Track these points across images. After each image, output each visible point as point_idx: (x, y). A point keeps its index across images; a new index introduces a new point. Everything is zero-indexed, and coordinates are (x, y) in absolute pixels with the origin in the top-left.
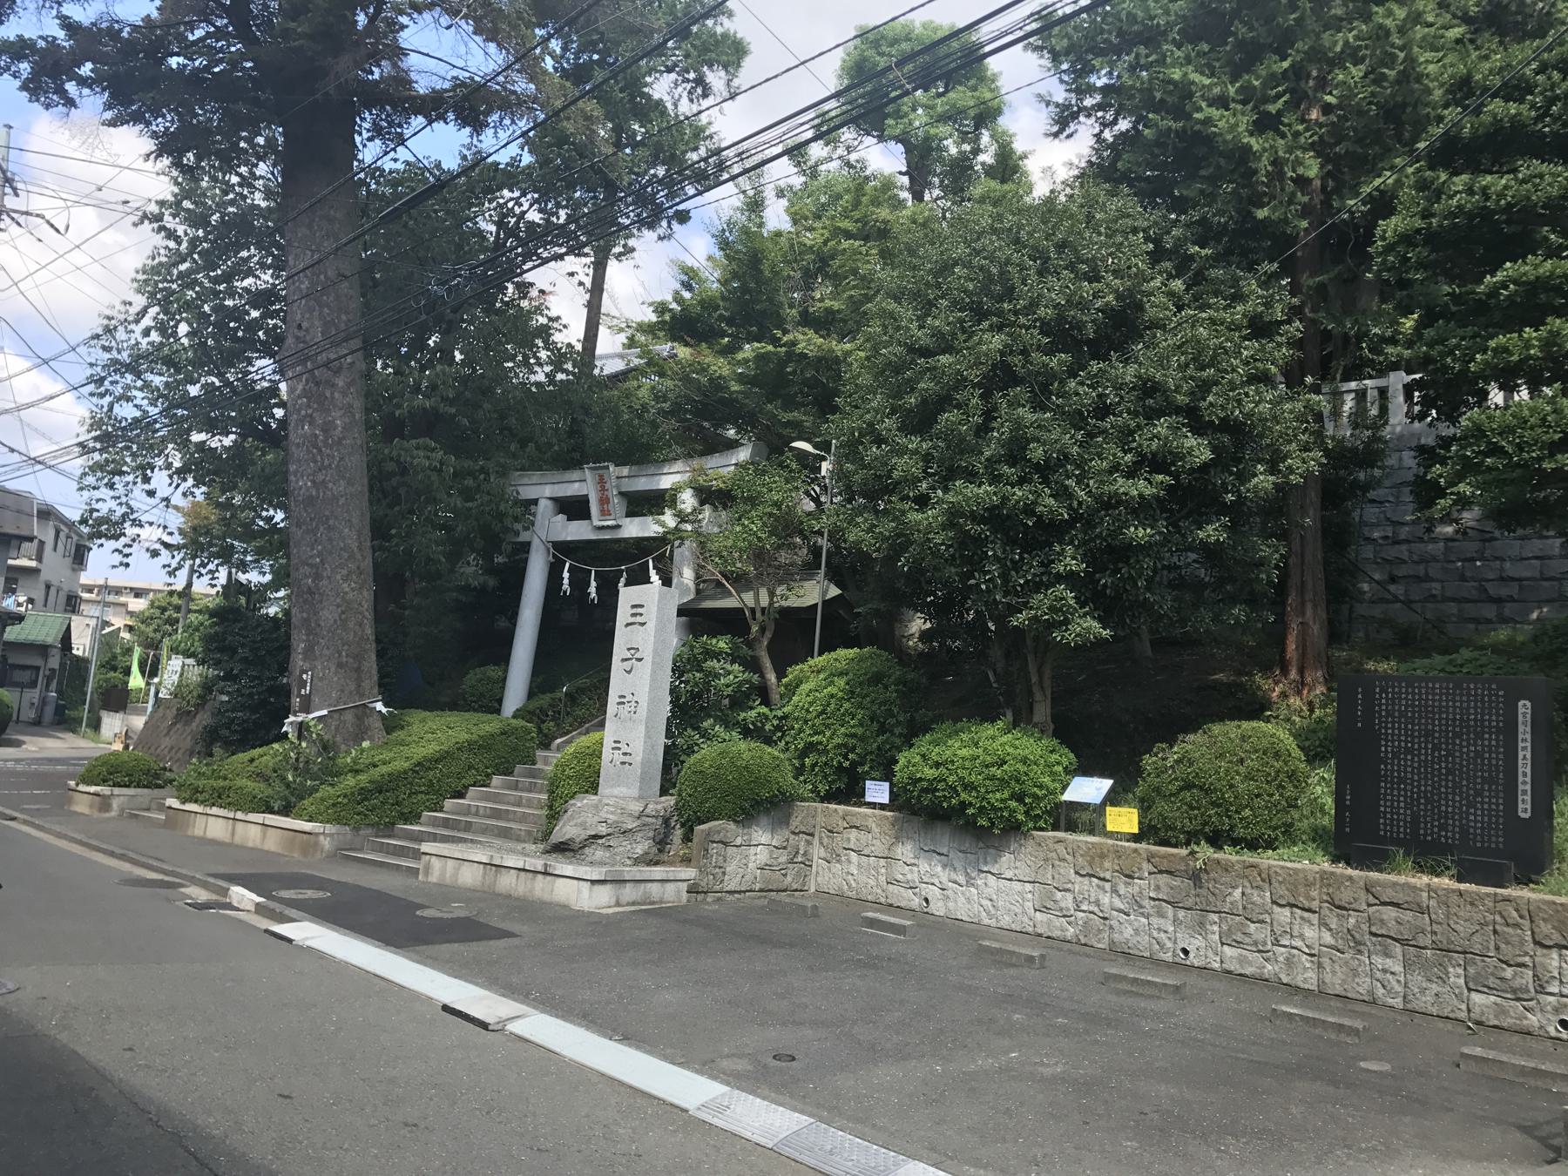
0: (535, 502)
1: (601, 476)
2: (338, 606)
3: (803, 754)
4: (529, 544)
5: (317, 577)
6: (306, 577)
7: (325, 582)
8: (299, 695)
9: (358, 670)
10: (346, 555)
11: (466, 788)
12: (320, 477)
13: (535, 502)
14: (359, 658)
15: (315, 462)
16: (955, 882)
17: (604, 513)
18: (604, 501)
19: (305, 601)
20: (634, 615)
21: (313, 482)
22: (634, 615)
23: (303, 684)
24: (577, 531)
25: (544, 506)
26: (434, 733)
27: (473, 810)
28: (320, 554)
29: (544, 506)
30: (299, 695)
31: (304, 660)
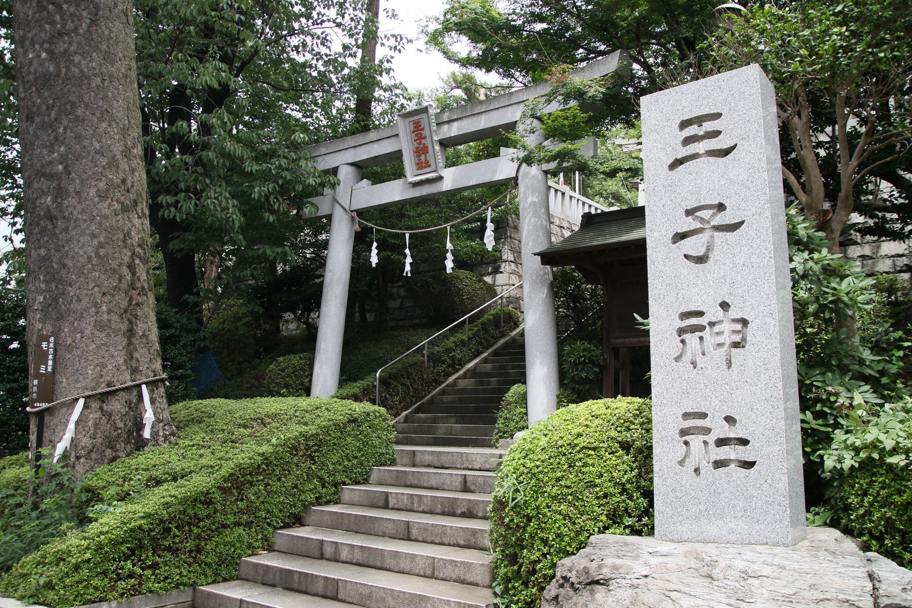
0: (335, 171)
1: (417, 125)
2: (94, 236)
3: (534, 438)
4: (329, 217)
5: (60, 193)
6: (43, 193)
7: (73, 201)
8: (38, 376)
9: (130, 333)
10: (104, 161)
11: (306, 507)
12: (61, 47)
13: (335, 171)
14: (130, 314)
15: (53, 23)
16: (847, 566)
17: (422, 165)
18: (421, 151)
19: (43, 231)
20: (687, 141)
21: (51, 53)
22: (687, 141)
23: (42, 357)
24: (392, 192)
25: (346, 173)
26: (252, 427)
27: (328, 551)
28: (63, 159)
29: (346, 173)
30: (38, 376)
31: (43, 321)
